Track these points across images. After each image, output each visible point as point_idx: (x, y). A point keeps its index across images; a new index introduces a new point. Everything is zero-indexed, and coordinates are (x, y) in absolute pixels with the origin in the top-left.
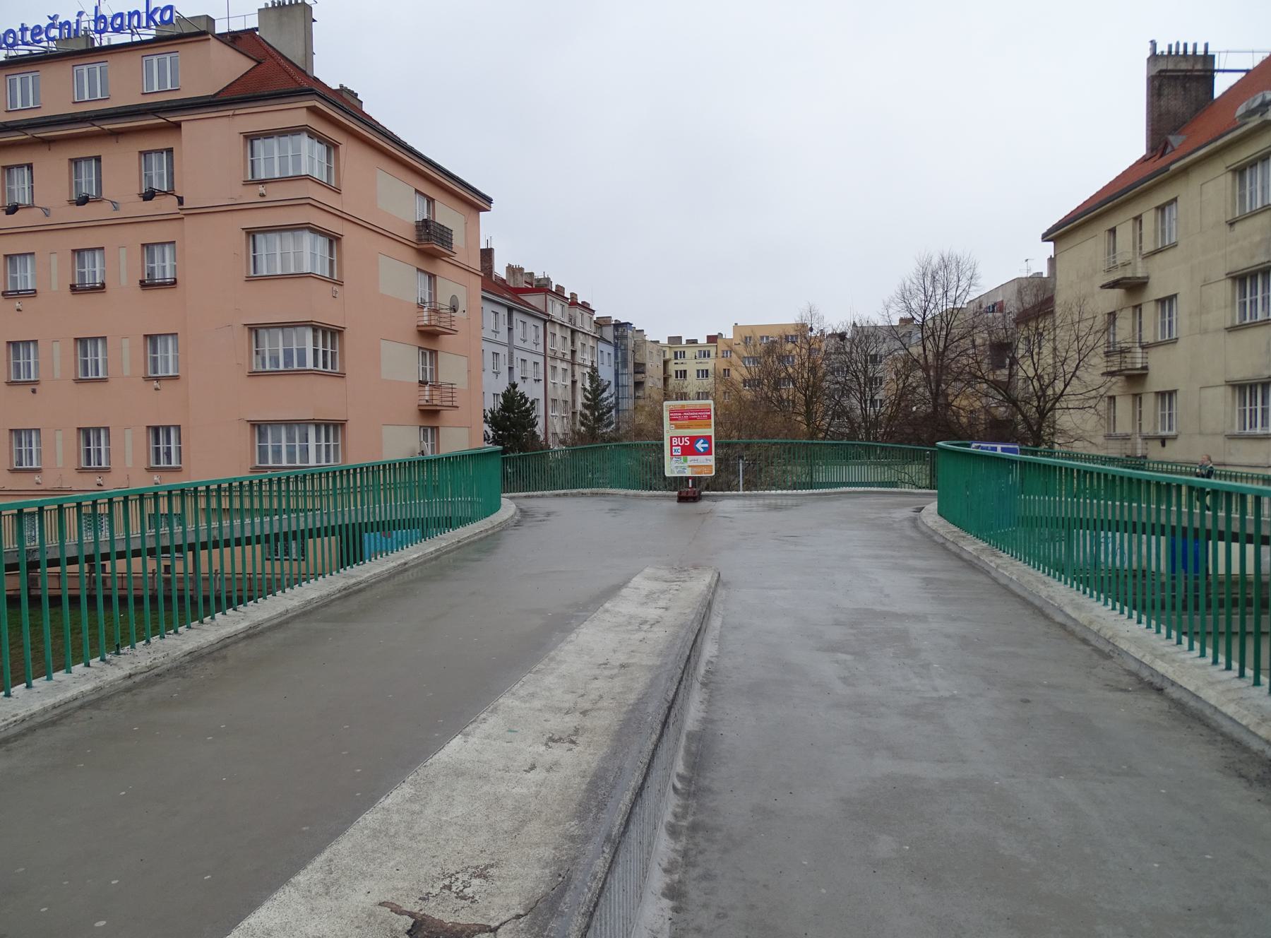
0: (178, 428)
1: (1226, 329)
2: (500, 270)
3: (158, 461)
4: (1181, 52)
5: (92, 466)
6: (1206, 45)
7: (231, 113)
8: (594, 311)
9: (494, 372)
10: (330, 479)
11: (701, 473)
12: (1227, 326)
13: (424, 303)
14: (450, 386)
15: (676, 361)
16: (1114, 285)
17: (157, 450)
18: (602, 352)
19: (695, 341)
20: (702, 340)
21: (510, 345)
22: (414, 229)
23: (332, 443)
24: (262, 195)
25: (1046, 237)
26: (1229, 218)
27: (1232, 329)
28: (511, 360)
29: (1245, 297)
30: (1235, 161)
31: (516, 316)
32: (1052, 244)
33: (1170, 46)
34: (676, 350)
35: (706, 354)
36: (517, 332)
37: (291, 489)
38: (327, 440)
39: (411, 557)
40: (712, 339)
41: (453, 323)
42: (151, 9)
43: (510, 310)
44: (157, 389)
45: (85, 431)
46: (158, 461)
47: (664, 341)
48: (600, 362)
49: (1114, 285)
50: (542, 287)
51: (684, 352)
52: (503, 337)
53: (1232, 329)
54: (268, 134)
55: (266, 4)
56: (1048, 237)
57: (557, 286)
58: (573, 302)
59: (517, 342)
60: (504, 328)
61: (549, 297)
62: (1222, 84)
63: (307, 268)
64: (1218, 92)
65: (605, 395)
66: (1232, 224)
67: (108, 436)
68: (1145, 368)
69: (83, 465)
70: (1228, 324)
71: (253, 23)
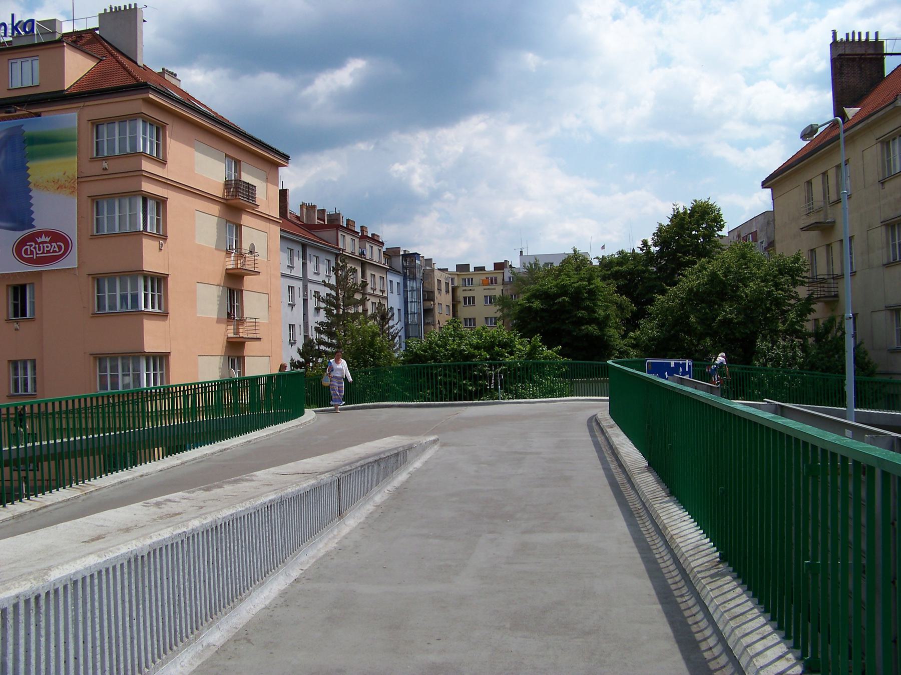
0: (34, 362)
1: (884, 265)
2: (294, 207)
3: (17, 390)
5: (20, 393)
6: (877, 33)
7: (82, 105)
8: (382, 243)
9: (289, 304)
10: (121, 406)
11: (823, 436)
12: (885, 263)
13: (232, 249)
14: (254, 320)
17: (16, 381)
18: (391, 281)
19: (483, 269)
20: (490, 268)
21: (305, 280)
22: (222, 188)
23: (159, 372)
24: (105, 169)
25: (765, 185)
26: (881, 178)
27: (887, 265)
28: (305, 295)
29: (899, 243)
31: (309, 251)
32: (769, 190)
35: (493, 281)
36: (311, 266)
37: (111, 411)
38: (155, 369)
39: (253, 438)
40: (499, 266)
41: (256, 265)
42: (16, 22)
43: (304, 247)
46: (17, 390)
47: (453, 269)
48: (389, 291)
50: (334, 223)
51: (472, 279)
52: (298, 272)
53: (887, 265)
54: (110, 121)
55: (105, 10)
56: (767, 185)
57: (348, 220)
58: (364, 238)
59: (311, 276)
60: (298, 262)
61: (340, 233)
64: (887, 71)
65: (391, 323)
66: (882, 183)
67: (34, 368)
68: (836, 296)
69: (12, 392)
70: (885, 262)
71: (94, 23)
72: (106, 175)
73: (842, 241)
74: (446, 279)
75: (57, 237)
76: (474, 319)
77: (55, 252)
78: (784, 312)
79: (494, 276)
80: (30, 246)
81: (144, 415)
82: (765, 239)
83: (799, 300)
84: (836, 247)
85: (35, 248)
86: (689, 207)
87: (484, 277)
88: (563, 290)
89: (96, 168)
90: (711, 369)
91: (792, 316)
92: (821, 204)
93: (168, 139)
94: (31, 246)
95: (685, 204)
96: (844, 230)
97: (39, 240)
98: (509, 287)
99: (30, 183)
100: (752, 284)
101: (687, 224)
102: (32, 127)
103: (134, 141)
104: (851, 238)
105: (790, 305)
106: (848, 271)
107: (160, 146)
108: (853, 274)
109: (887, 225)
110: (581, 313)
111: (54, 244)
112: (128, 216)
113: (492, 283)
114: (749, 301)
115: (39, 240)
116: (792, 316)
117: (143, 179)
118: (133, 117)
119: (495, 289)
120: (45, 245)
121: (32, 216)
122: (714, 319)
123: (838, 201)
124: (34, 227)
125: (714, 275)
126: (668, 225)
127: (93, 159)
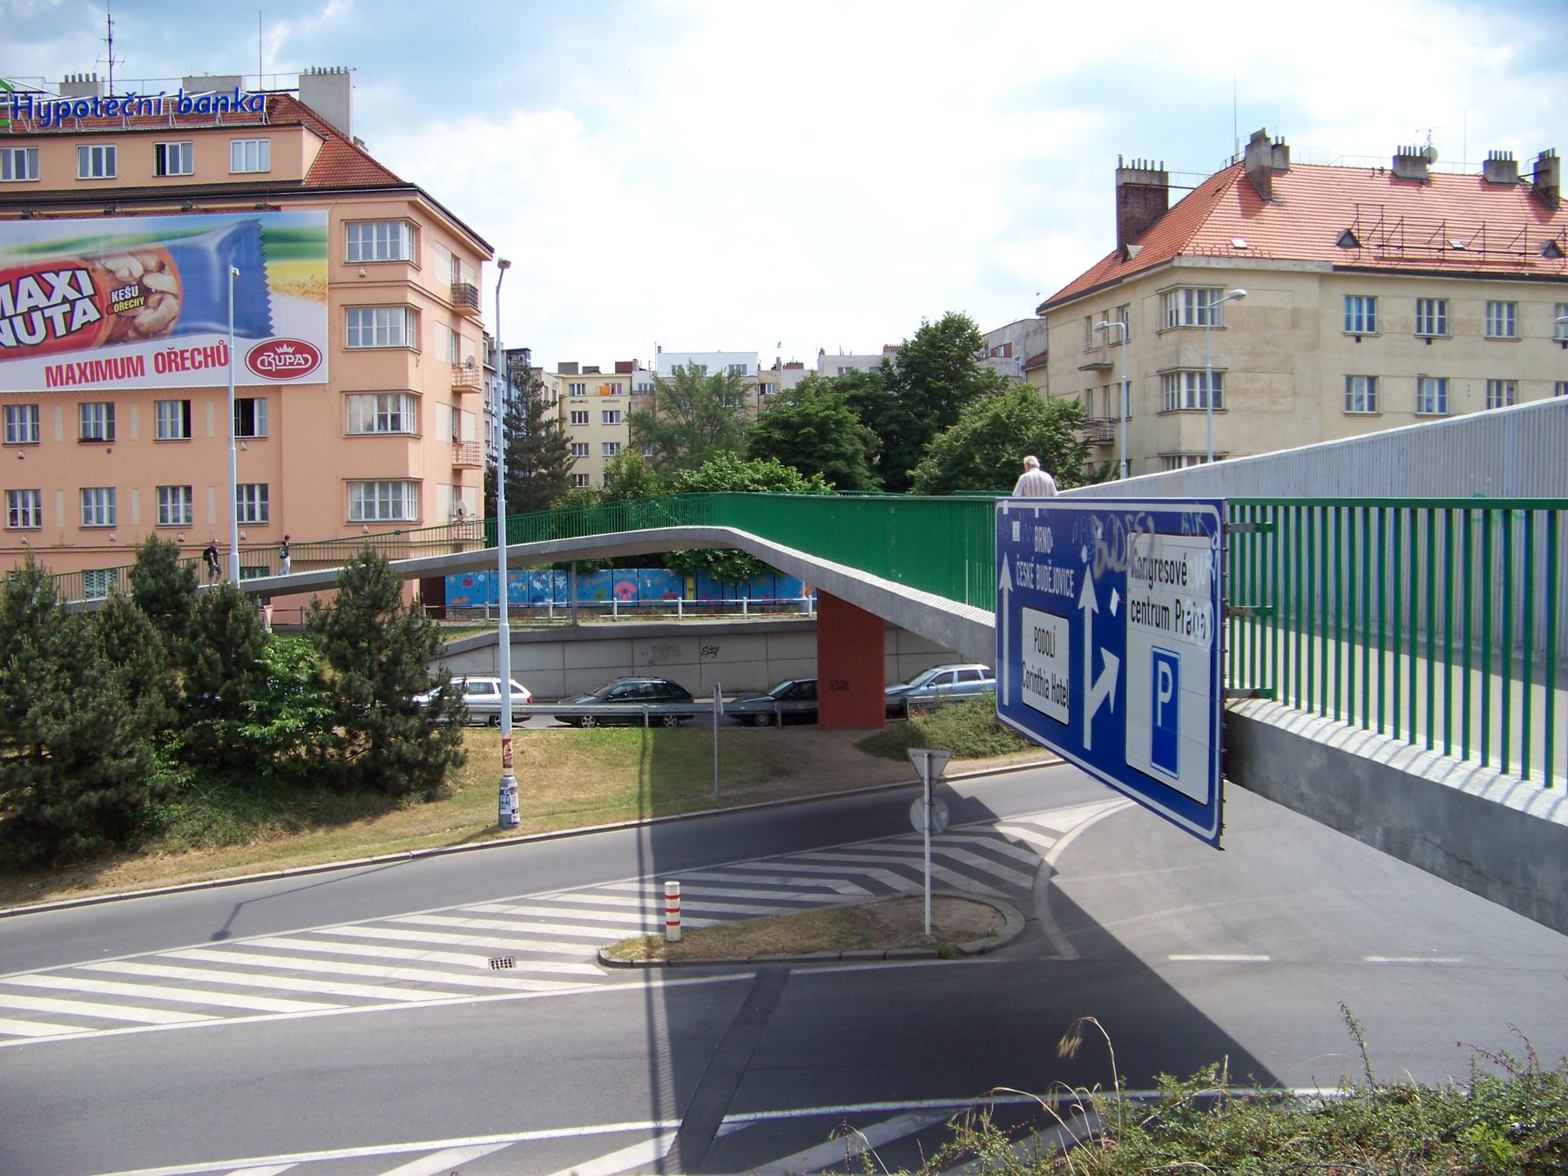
4: (1142, 168)
7: (334, 201)
15: (573, 399)
16: (1088, 368)
19: (595, 370)
20: (608, 368)
22: (449, 291)
27: (1162, 414)
30: (1168, 284)
33: (1133, 161)
34: (572, 382)
35: (614, 390)
40: (624, 368)
44: (21, 458)
45: (85, 491)
49: (1088, 368)
53: (1162, 414)
62: (1174, 198)
63: (402, 343)
66: (1160, 334)
68: (1112, 440)
72: (362, 284)
73: (1120, 384)
74: (554, 385)
75: (301, 348)
76: (587, 445)
77: (300, 364)
78: (1061, 455)
79: (616, 381)
80: (268, 357)
81: (410, 546)
82: (1022, 355)
83: (1076, 445)
84: (1113, 390)
85: (274, 359)
86: (941, 318)
87: (601, 383)
88: (807, 420)
89: (351, 275)
90: (411, 699)
91: (1071, 460)
92: (1101, 344)
93: (423, 245)
94: (269, 356)
95: (935, 318)
96: (1121, 375)
97: (279, 351)
98: (639, 398)
99: (267, 285)
100: (1034, 427)
101: (939, 342)
102: (269, 222)
103: (396, 246)
104: (1128, 384)
105: (1067, 448)
106: (1124, 416)
107: (417, 250)
108: (1129, 419)
109: (1162, 375)
110: (829, 447)
111: (298, 356)
112: (388, 330)
113: (613, 392)
114: (1030, 444)
115: (279, 351)
116: (1071, 460)
117: (409, 289)
118: (395, 221)
119: (618, 401)
120: (287, 356)
121: (271, 323)
122: (997, 461)
123: (1118, 344)
124: (272, 335)
125: (997, 416)
126: (914, 341)
127: (347, 264)
